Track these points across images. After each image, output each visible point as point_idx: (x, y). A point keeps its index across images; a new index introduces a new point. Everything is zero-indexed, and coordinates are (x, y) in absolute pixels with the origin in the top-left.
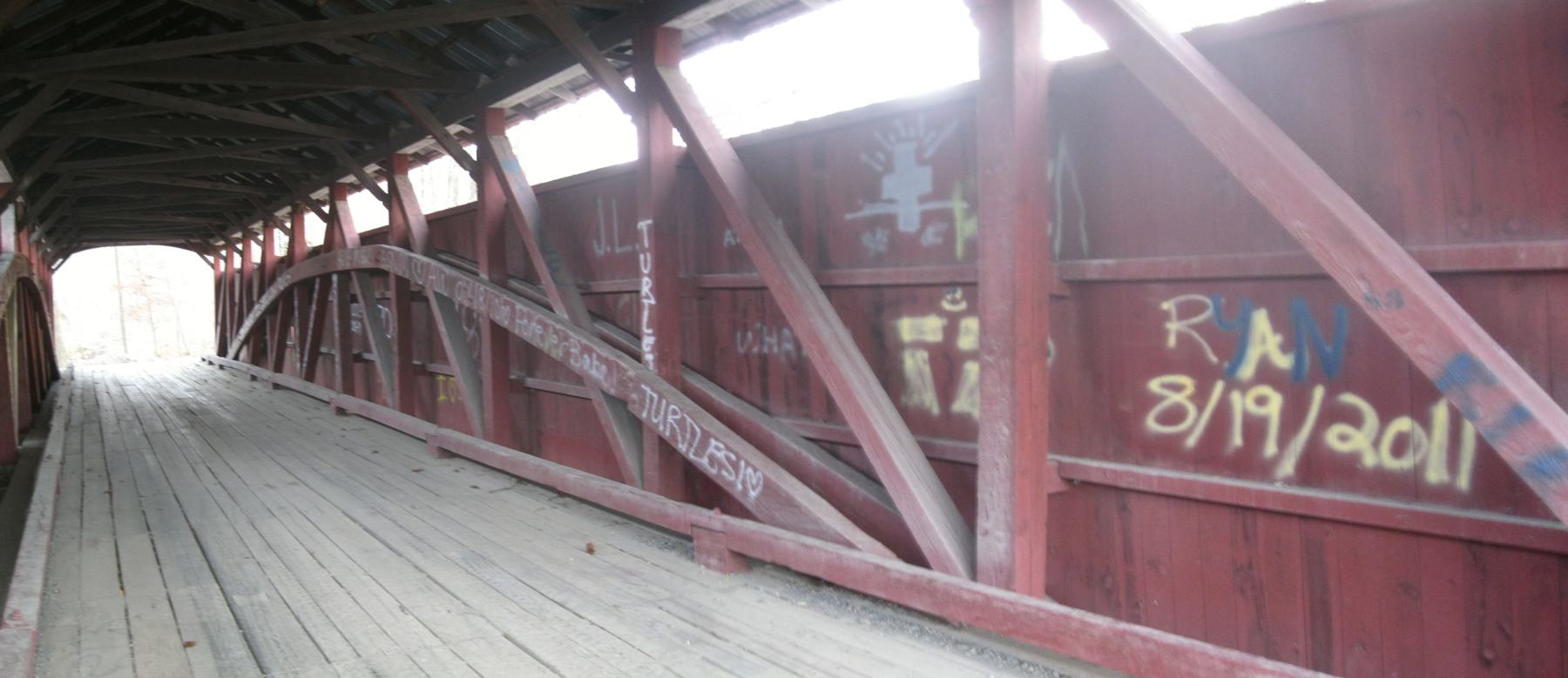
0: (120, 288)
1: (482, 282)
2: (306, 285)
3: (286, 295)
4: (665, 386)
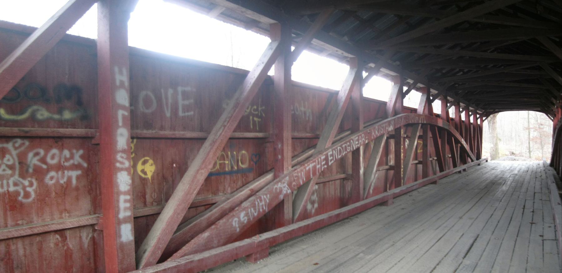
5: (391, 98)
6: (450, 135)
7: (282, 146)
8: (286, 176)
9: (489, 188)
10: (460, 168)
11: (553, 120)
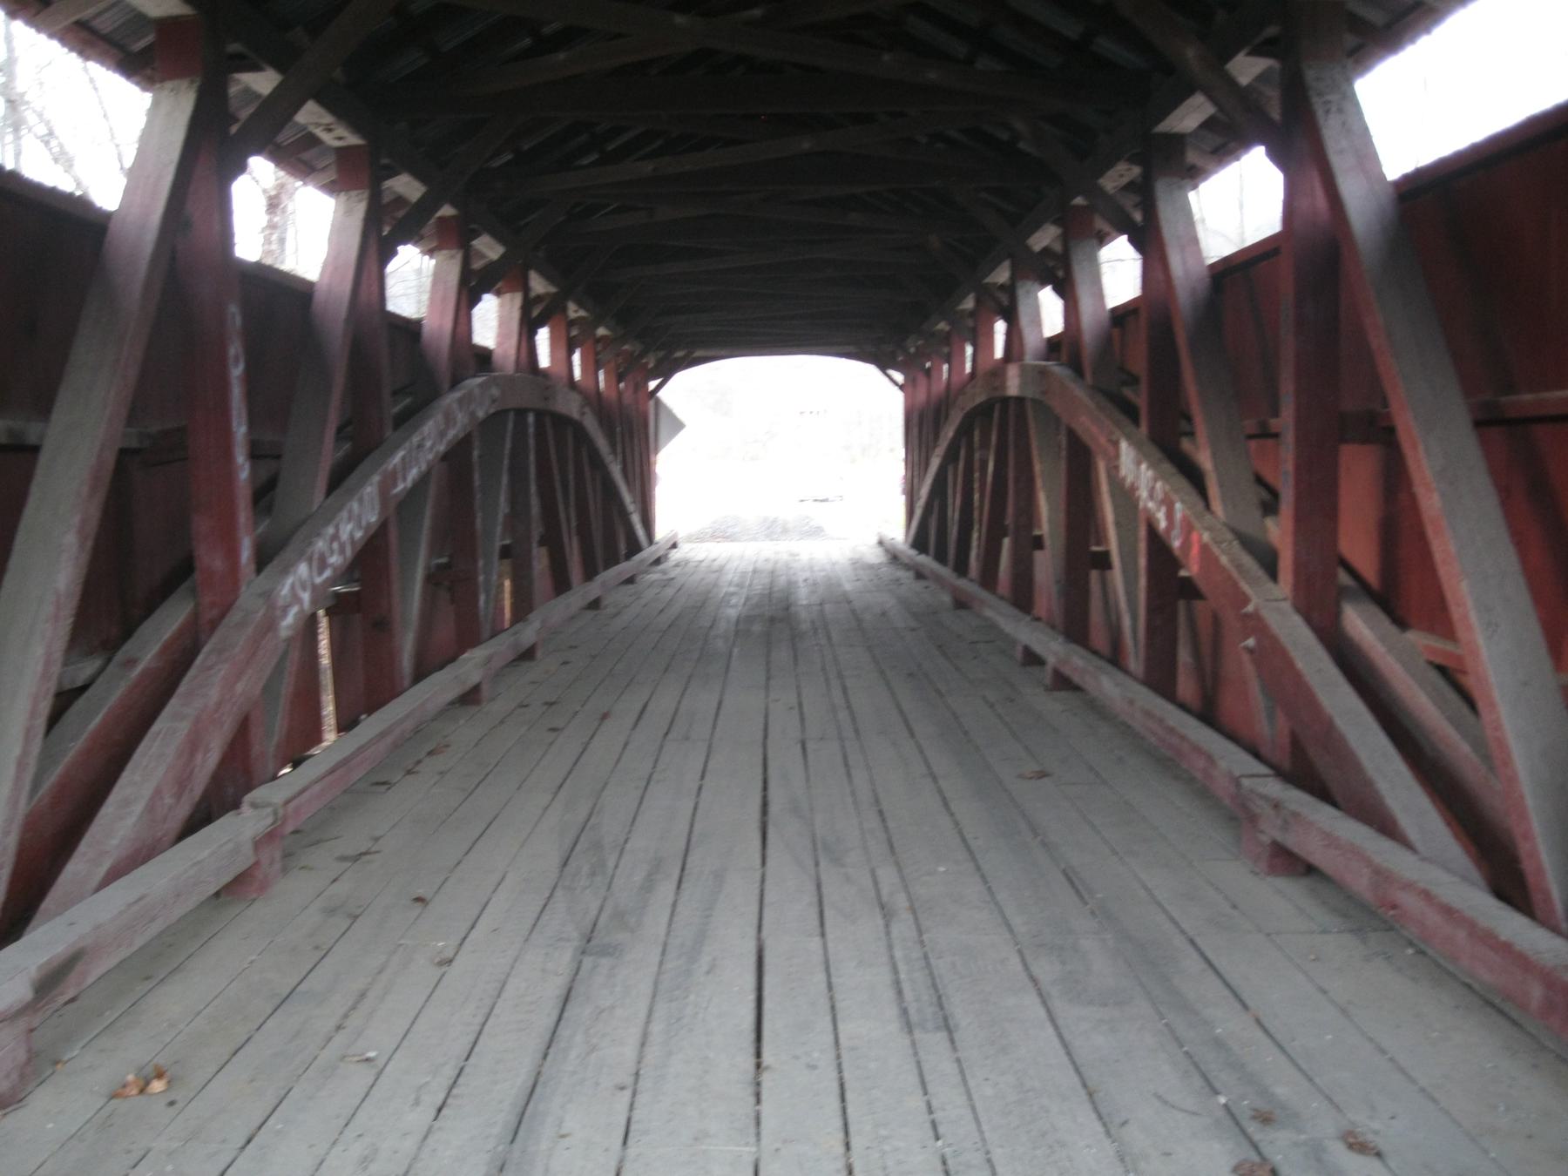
2: (982, 413)
3: (965, 431)
5: (502, 336)
9: (778, 626)
11: (901, 387)
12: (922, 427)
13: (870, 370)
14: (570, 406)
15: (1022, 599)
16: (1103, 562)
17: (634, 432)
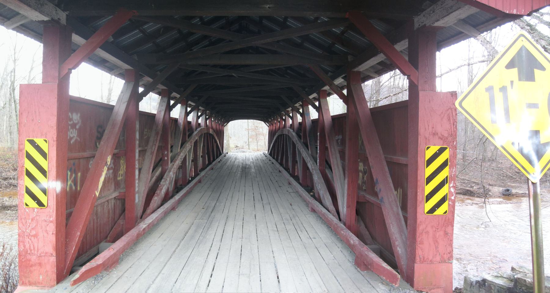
0: (248, 130)
1: (300, 142)
4: (319, 171)
6: (213, 138)
7: (168, 152)
8: (171, 169)
9: (245, 170)
10: (218, 160)
12: (272, 134)
13: (263, 123)
14: (211, 131)
15: (277, 160)
16: (297, 162)
17: (220, 134)
